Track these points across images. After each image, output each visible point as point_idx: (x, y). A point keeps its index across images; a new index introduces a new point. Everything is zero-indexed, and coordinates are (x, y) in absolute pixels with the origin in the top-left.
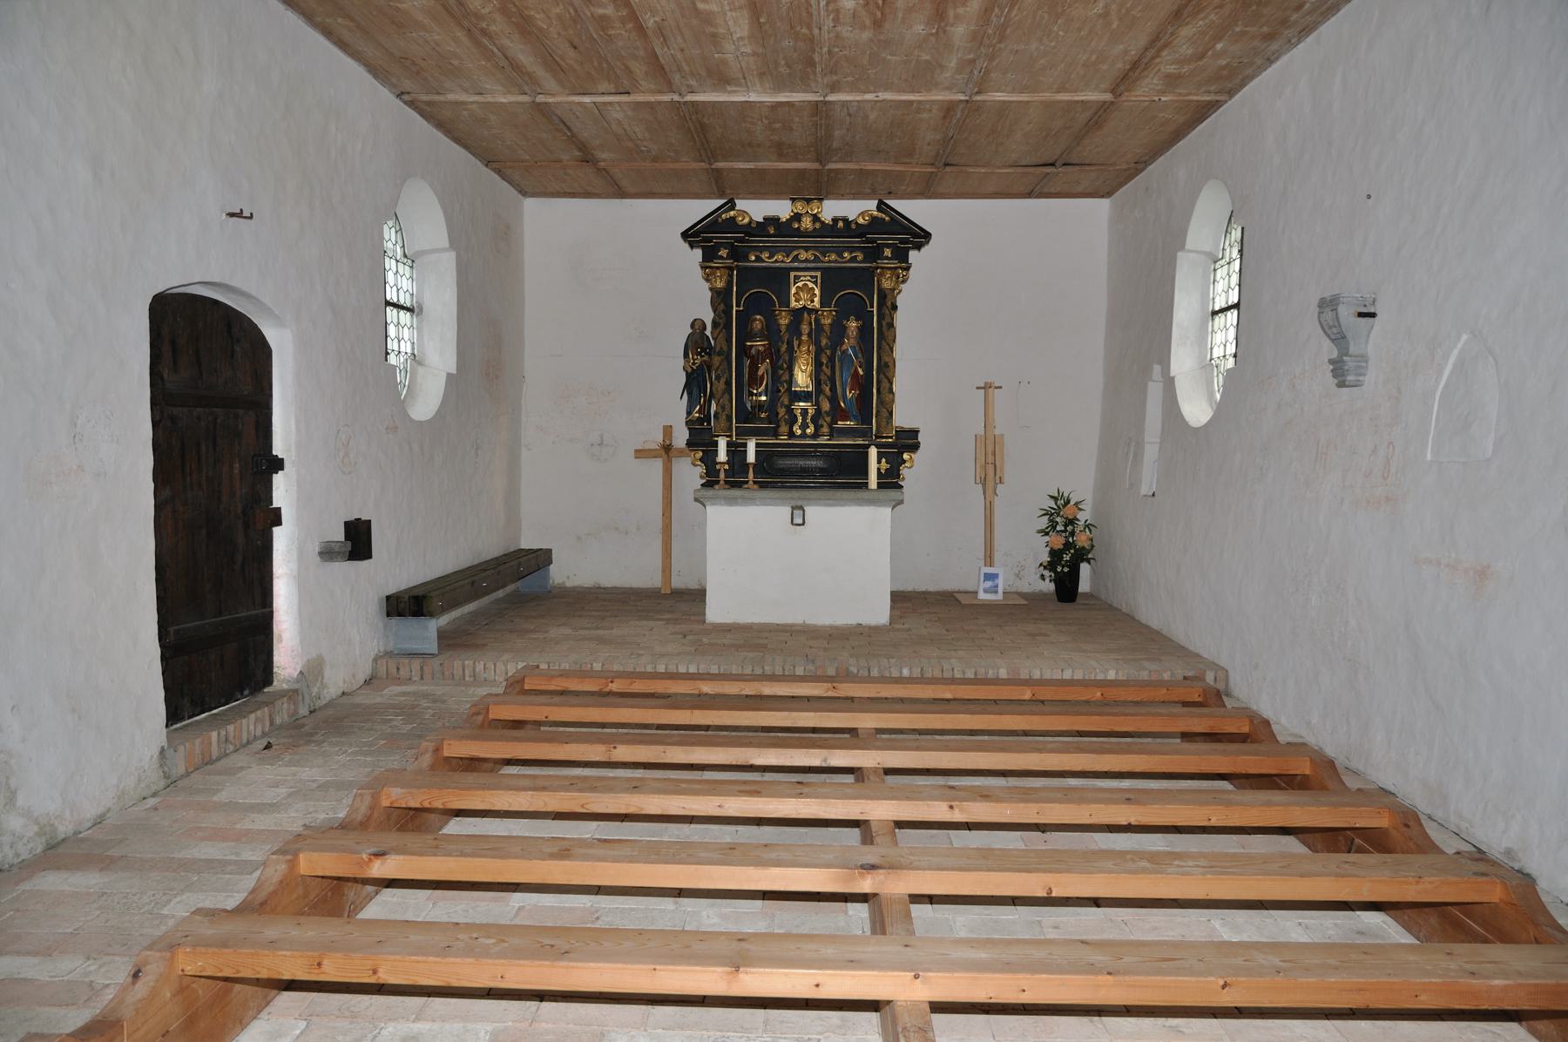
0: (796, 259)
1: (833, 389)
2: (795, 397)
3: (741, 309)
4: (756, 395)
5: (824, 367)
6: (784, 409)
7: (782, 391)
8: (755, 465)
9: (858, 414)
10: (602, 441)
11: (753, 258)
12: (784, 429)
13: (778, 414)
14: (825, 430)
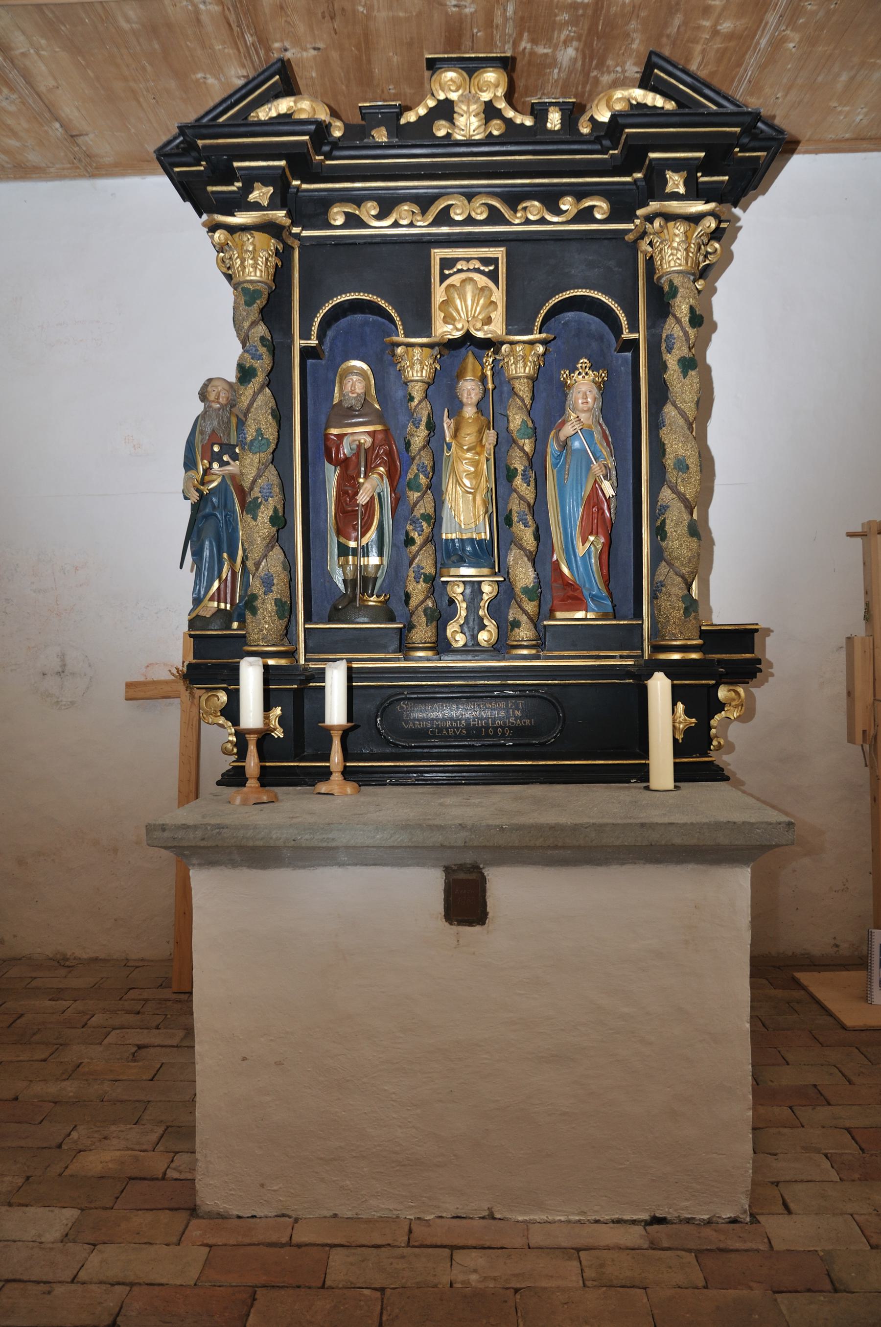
0: (444, 217)
1: (541, 534)
2: (449, 556)
3: (314, 342)
4: (354, 552)
5: (518, 481)
6: (422, 586)
7: (419, 540)
8: (345, 734)
9: (605, 594)
10: (64, 666)
11: (340, 220)
12: (422, 633)
13: (408, 597)
14: (525, 633)
